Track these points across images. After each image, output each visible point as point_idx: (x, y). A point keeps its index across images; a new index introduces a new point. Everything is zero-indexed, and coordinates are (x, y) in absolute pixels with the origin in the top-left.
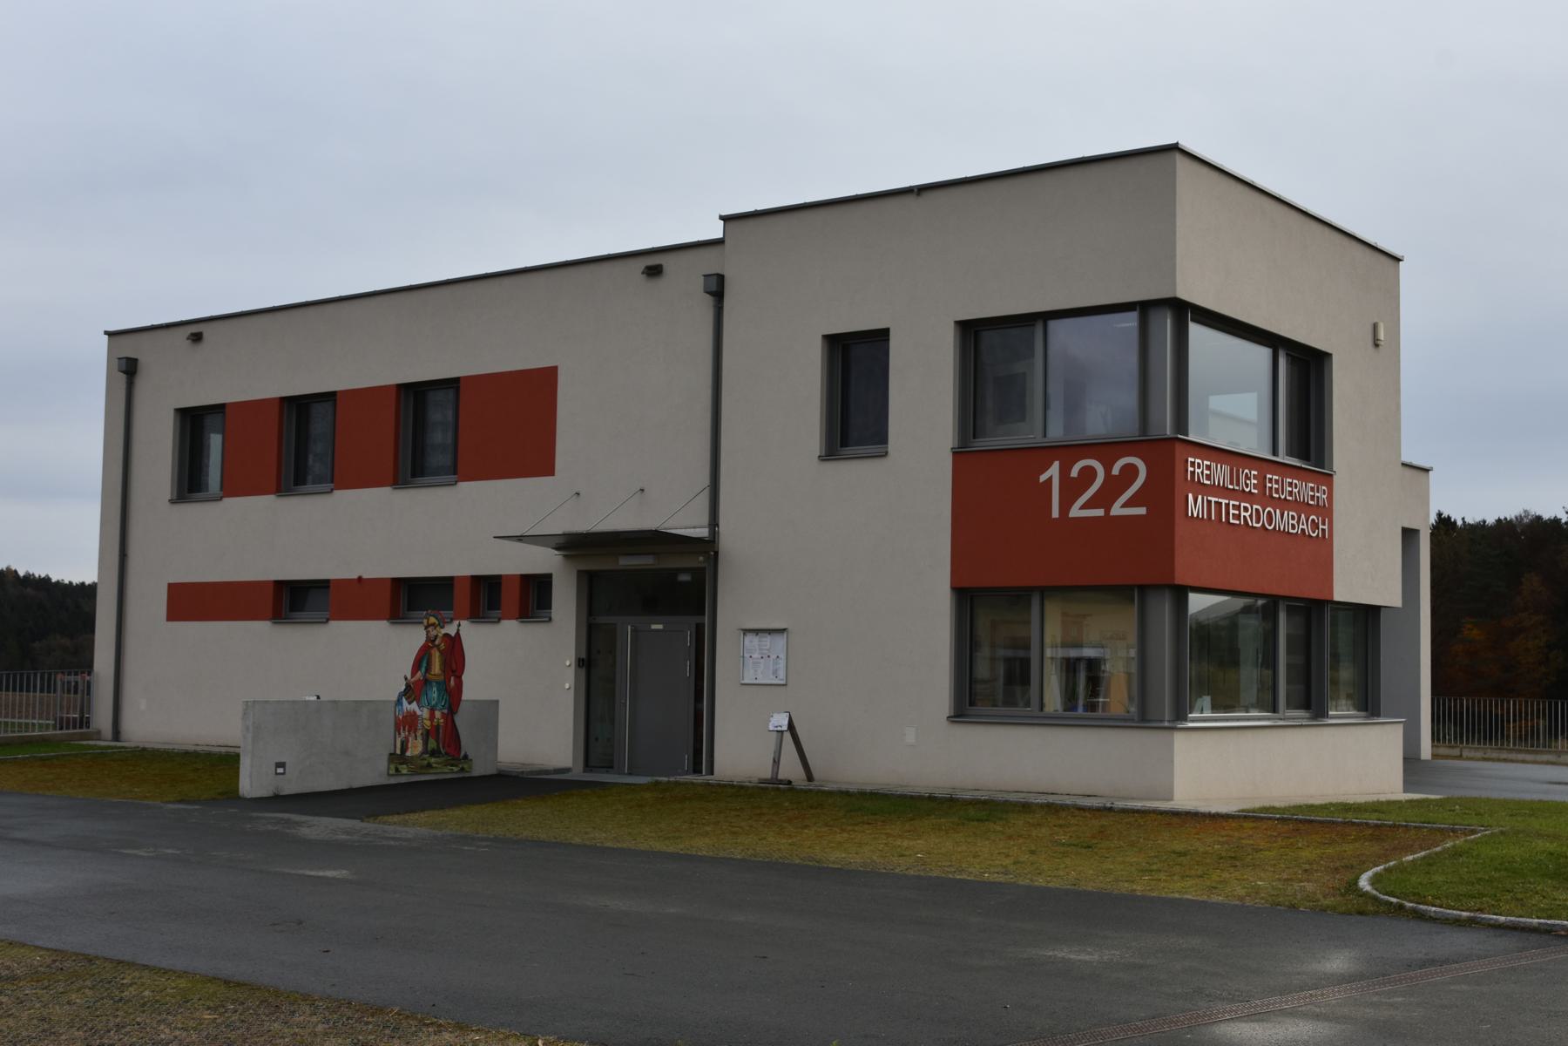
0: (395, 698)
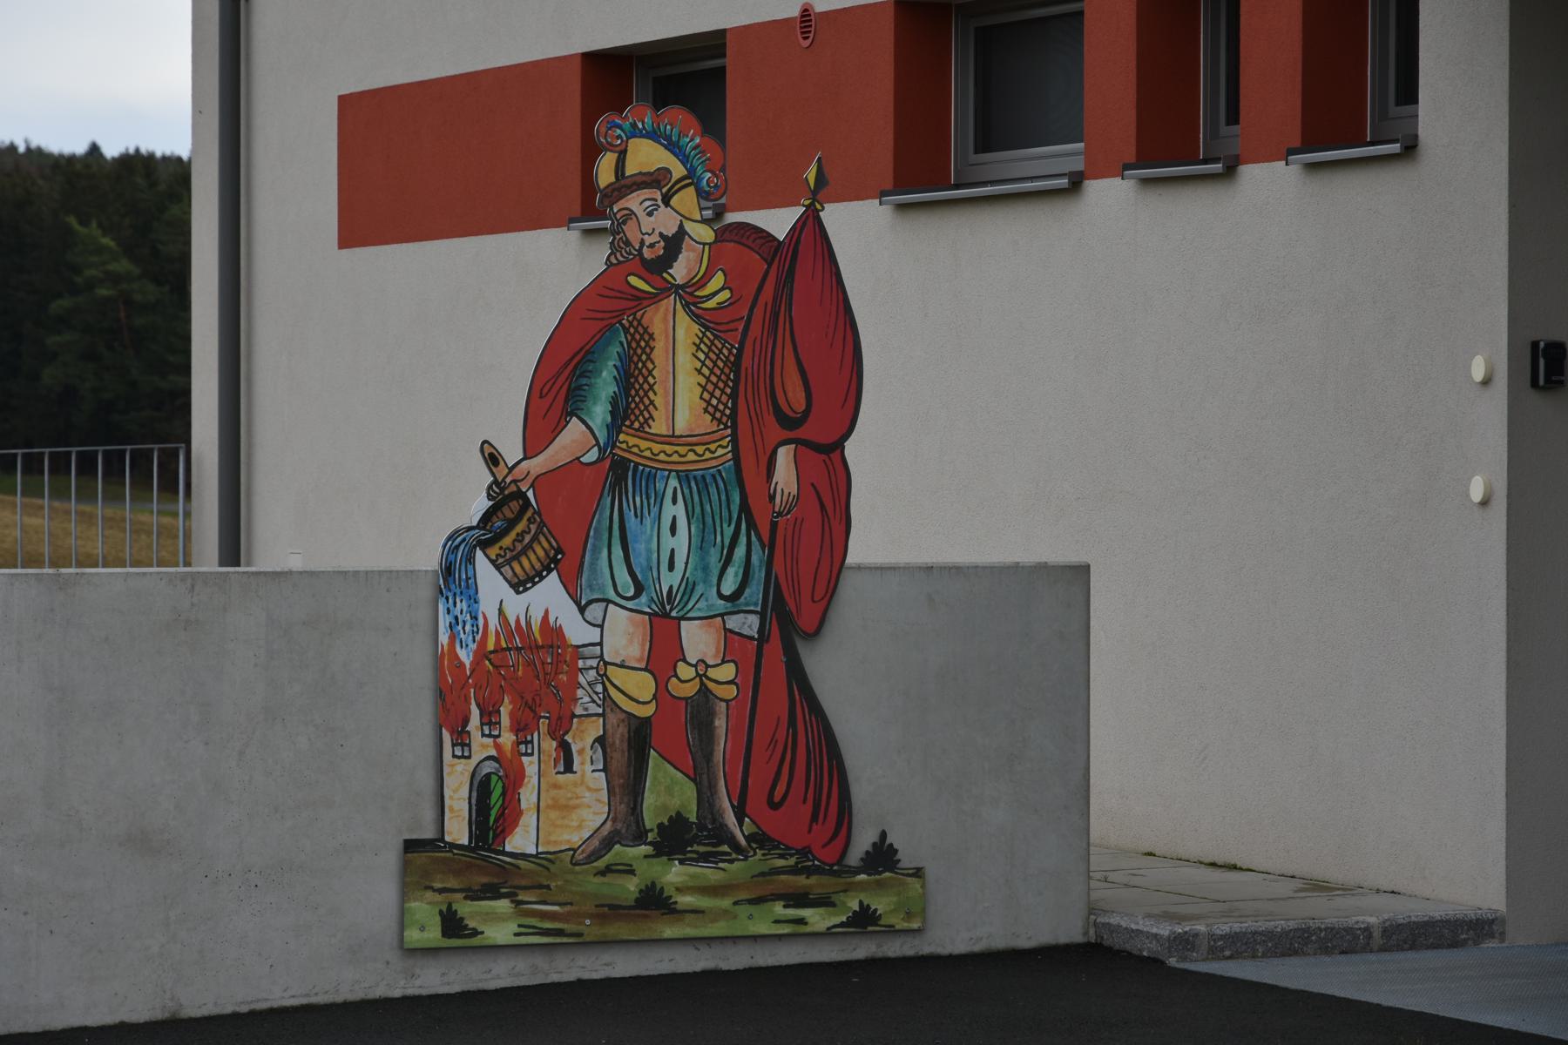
0: (429, 559)
